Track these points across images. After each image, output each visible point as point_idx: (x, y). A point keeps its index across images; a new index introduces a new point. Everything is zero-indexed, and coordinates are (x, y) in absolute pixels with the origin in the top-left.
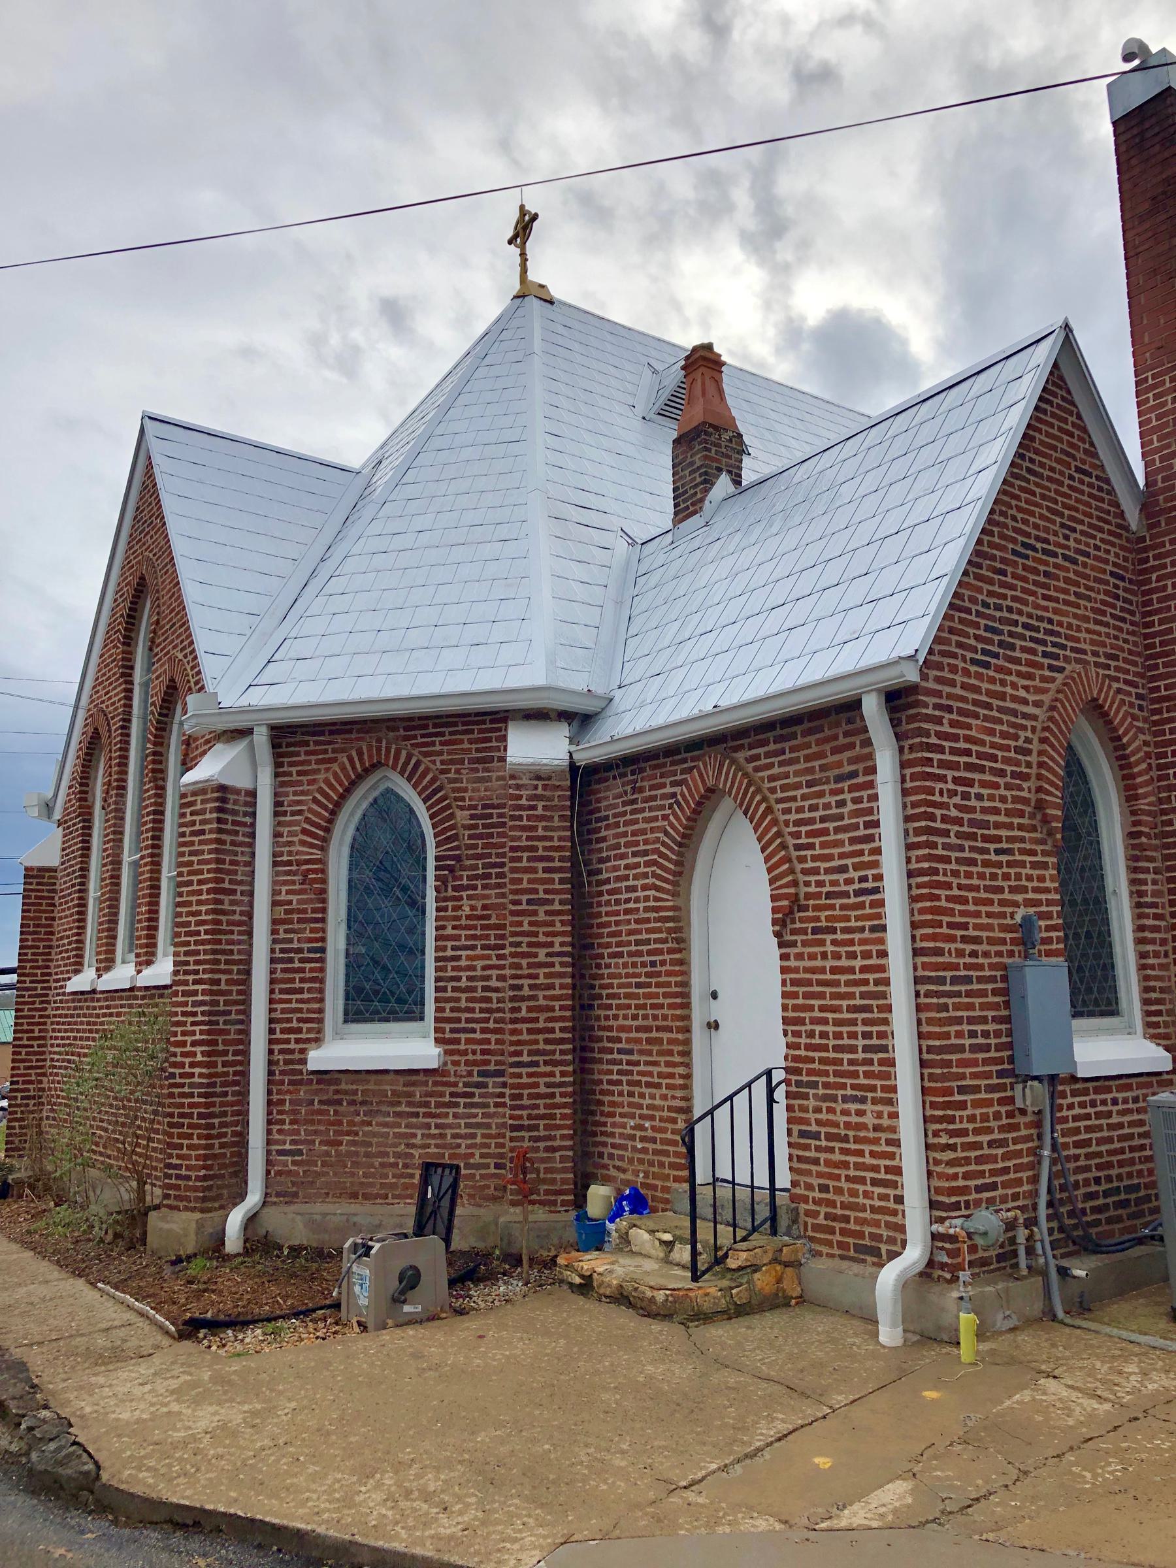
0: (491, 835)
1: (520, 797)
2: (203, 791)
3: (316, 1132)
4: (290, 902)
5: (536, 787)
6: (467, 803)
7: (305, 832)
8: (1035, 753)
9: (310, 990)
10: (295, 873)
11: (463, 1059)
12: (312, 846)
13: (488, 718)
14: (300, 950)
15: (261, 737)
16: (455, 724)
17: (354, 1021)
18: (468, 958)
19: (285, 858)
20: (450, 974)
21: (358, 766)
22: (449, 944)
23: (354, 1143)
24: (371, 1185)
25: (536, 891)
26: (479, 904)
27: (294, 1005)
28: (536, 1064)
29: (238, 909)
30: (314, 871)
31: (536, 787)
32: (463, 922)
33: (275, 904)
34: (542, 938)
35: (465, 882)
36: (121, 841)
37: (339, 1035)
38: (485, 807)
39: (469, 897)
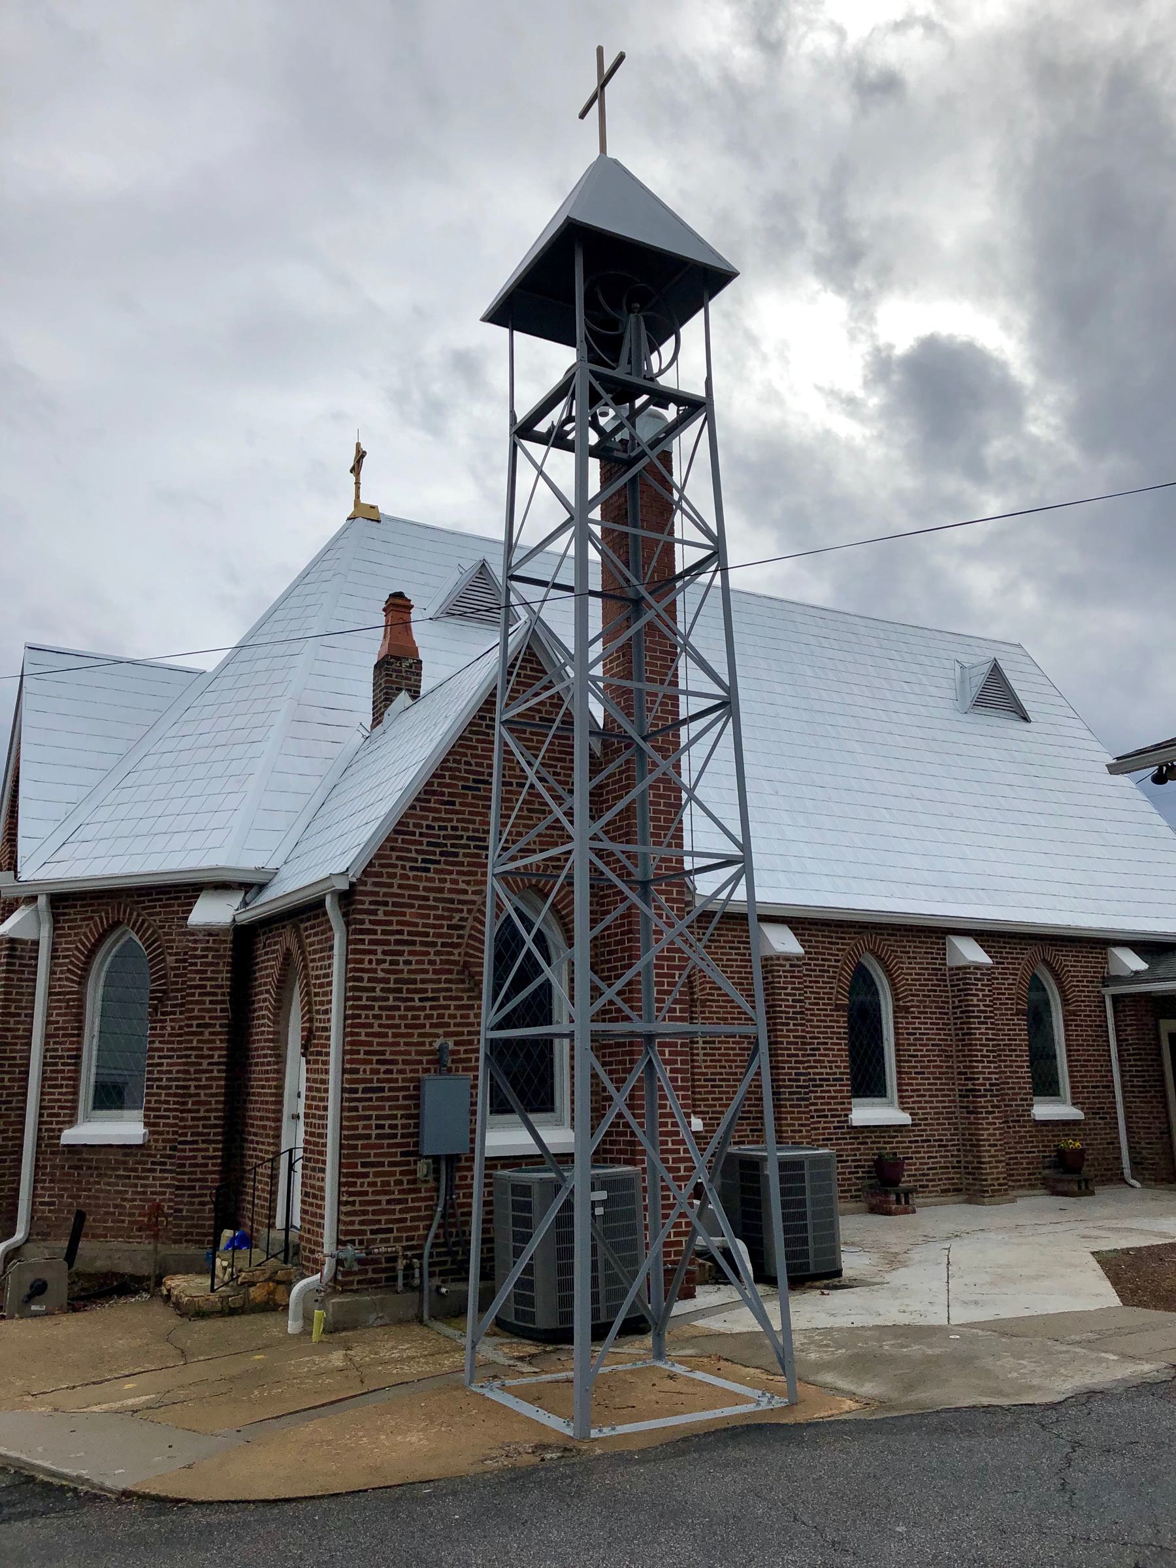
1: (196, 949)
3: (65, 1189)
4: (58, 1022)
5: (208, 942)
6: (175, 951)
8: (468, 928)
9: (67, 1086)
11: (161, 1137)
12: (73, 981)
15: (42, 901)
16: (170, 893)
17: (101, 1108)
19: (57, 990)
20: (156, 1076)
22: (157, 1054)
23: (88, 1197)
24: (98, 1227)
25: (203, 1018)
27: (56, 1097)
28: (196, 1142)
29: (21, 1027)
31: (208, 942)
33: (48, 1023)
34: (206, 1052)
35: (169, 1009)
37: (88, 1119)
39: (172, 1020)
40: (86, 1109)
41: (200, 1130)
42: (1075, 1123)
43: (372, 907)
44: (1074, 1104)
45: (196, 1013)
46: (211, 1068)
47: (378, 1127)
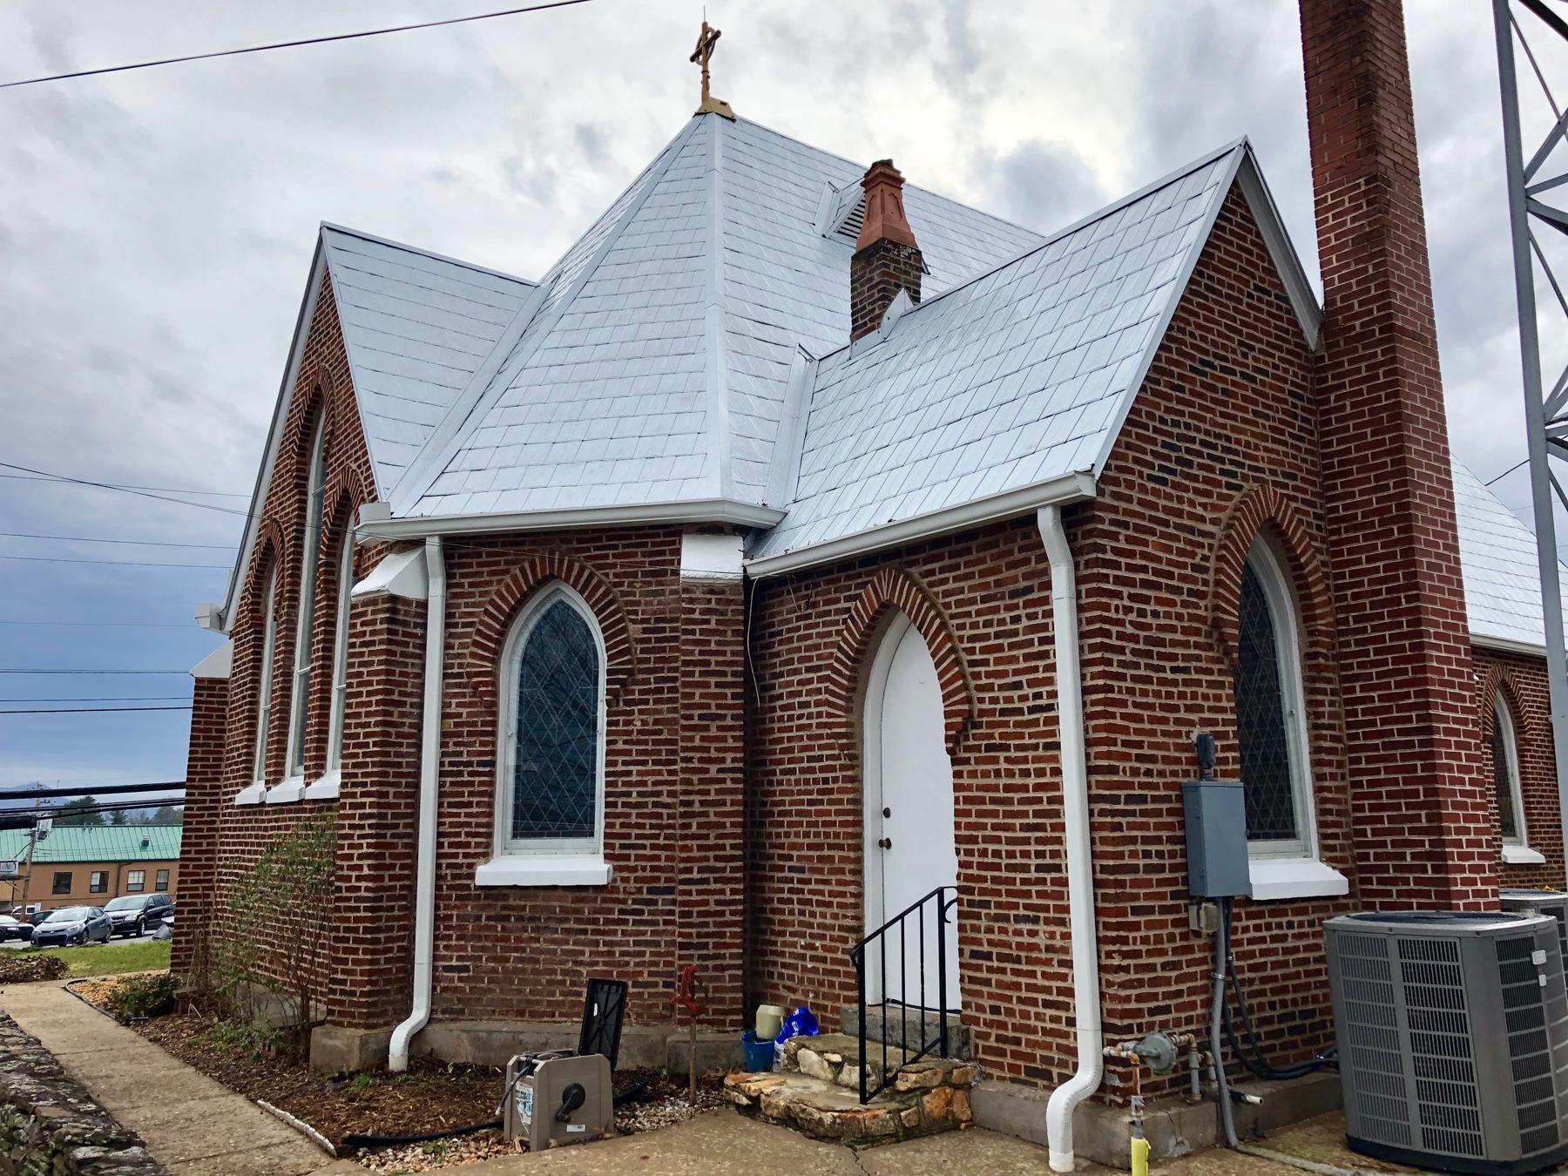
0: (663, 650)
1: (693, 611)
2: (374, 602)
3: (483, 949)
4: (460, 715)
5: (709, 601)
6: (640, 617)
7: (476, 644)
8: (1212, 572)
9: (479, 804)
10: (465, 686)
11: (632, 875)
12: (483, 658)
13: (661, 531)
14: (469, 764)
15: (433, 547)
16: (629, 537)
18: (639, 773)
19: (456, 670)
20: (621, 789)
21: (531, 578)
22: (620, 759)
24: (538, 1002)
25: (708, 706)
26: (651, 719)
27: (462, 819)
28: (706, 881)
29: (407, 721)
30: (485, 684)
31: (709, 601)
32: (634, 737)
33: (445, 716)
34: (713, 754)
35: (637, 696)
36: (292, 652)
37: (506, 849)
38: (658, 620)
39: (641, 712)
40: (504, 839)
41: (712, 863)
42: (1537, 866)
43: (1113, 529)
44: (1531, 846)
45: (697, 700)
46: (721, 776)
47: (1039, 854)
